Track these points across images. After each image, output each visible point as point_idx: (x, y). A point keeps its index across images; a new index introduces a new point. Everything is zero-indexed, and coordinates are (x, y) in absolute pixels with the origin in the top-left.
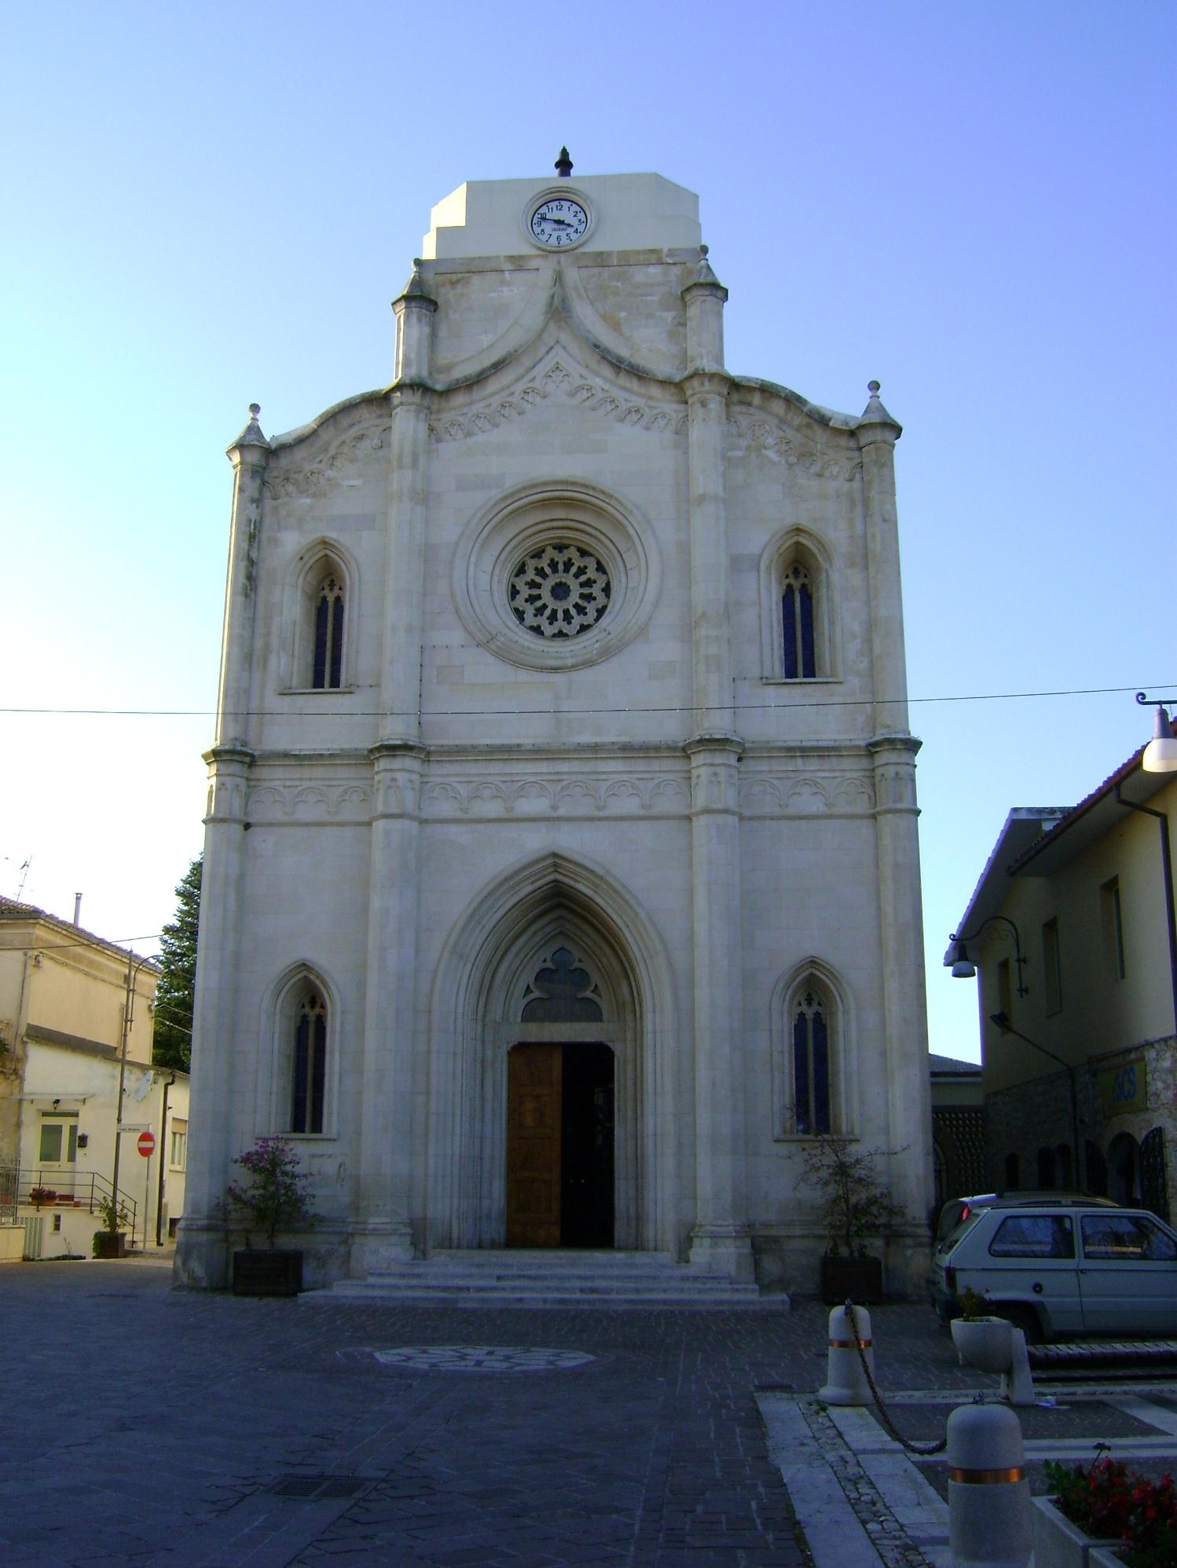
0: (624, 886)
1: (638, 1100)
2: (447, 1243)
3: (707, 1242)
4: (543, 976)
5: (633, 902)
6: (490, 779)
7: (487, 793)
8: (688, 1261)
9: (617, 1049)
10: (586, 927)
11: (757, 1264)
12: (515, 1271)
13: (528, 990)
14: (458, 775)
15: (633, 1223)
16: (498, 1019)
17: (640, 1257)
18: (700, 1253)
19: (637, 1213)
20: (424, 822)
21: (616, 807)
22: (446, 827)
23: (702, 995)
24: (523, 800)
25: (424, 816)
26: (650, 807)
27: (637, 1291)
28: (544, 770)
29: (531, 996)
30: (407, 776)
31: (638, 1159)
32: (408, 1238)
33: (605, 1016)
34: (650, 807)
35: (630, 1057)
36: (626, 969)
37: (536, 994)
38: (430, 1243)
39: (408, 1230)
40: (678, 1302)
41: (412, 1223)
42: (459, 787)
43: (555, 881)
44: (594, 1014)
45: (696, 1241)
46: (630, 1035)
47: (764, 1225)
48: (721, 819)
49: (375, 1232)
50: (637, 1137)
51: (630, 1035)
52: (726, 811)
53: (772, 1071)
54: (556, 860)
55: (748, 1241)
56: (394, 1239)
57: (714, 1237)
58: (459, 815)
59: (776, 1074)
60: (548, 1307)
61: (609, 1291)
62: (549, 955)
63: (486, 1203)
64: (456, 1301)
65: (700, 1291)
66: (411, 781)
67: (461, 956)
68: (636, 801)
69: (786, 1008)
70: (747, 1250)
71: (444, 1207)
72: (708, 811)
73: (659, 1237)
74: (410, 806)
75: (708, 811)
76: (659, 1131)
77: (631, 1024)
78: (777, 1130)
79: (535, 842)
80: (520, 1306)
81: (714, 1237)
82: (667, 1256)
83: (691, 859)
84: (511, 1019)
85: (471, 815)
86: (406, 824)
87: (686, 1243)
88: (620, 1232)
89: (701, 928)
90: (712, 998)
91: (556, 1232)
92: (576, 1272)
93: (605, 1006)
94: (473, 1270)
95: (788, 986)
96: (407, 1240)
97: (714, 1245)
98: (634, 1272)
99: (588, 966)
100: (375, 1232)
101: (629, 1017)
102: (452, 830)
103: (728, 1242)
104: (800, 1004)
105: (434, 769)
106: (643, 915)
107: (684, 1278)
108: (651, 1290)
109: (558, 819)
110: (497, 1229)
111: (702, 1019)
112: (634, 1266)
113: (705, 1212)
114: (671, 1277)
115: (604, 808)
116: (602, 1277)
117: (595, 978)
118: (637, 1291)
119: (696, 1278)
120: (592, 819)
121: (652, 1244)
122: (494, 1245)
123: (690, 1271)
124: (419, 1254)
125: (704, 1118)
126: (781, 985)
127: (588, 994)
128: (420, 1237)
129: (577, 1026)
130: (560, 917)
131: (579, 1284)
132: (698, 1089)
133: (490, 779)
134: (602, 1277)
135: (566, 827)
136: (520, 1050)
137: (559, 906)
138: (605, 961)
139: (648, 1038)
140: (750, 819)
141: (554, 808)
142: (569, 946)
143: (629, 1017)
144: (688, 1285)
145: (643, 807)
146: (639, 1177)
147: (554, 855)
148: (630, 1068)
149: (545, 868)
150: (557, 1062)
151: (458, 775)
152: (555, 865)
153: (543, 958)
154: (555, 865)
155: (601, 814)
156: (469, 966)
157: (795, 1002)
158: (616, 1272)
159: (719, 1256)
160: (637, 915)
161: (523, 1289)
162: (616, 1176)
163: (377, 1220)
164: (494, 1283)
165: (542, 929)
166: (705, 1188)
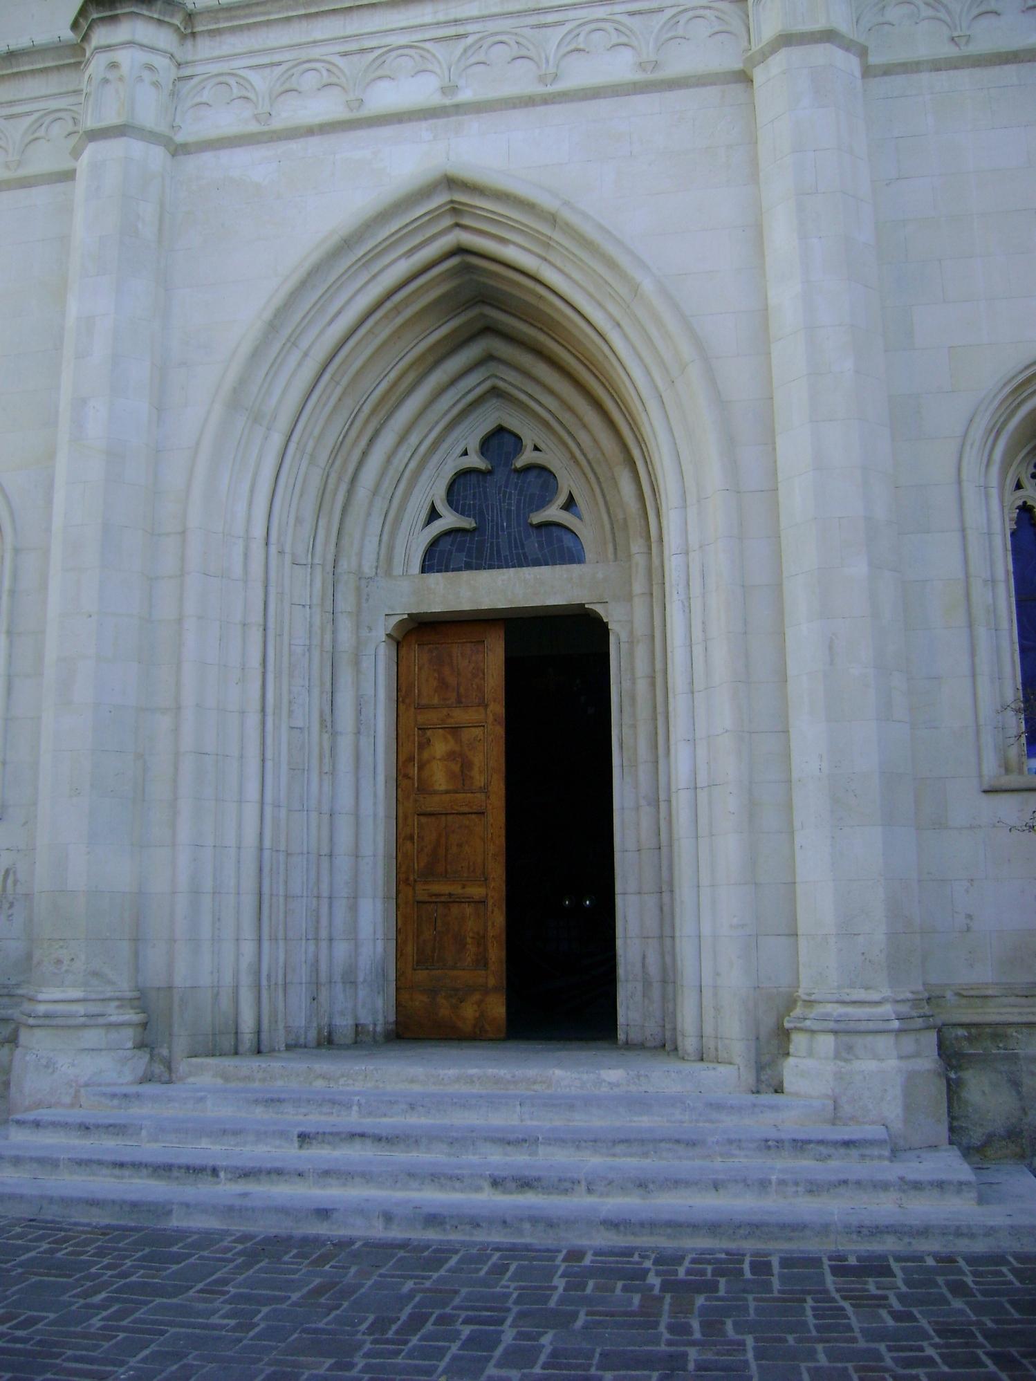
0: (602, 228)
1: (659, 715)
2: (224, 1043)
3: (826, 1043)
4: (461, 487)
5: (623, 260)
6: (316, 52)
7: (310, 81)
8: (779, 1090)
9: (613, 616)
10: (542, 370)
11: (953, 1090)
12: (353, 1119)
13: (433, 515)
14: (252, 53)
15: (656, 993)
16: (368, 570)
17: (662, 1077)
18: (809, 1070)
19: (664, 969)
20: (179, 150)
21: (580, 74)
22: (225, 156)
23: (794, 449)
24: (383, 85)
25: (180, 138)
26: (656, 65)
27: (642, 1185)
28: (428, 19)
29: (439, 526)
30: (143, 57)
31: (662, 848)
32: (129, 1033)
33: (589, 555)
34: (656, 65)
35: (640, 628)
36: (630, 453)
37: (449, 519)
38: (181, 1043)
39: (132, 1016)
40: (755, 1228)
41: (141, 1000)
42: (253, 77)
43: (460, 250)
44: (557, 546)
45: (799, 1041)
46: (638, 587)
47: (970, 996)
48: (822, 54)
49: (50, 1021)
50: (659, 800)
51: (638, 587)
52: (829, 36)
53: (970, 625)
54: (455, 193)
55: (932, 1037)
56: (92, 1037)
57: (845, 1031)
58: (254, 127)
59: (982, 632)
60: (396, 1233)
61: (565, 1184)
62: (473, 443)
63: (342, 949)
64: (162, 1210)
65: (814, 1188)
66: (150, 68)
67: (256, 419)
68: (627, 56)
69: (994, 479)
70: (928, 1062)
71: (214, 961)
72: (787, 40)
73: (708, 1029)
74: (149, 113)
75: (787, 40)
76: (702, 780)
77: (639, 560)
78: (990, 766)
79: (407, 161)
80: (320, 1229)
81: (845, 1031)
82: (727, 1077)
83: (754, 162)
84: (398, 570)
85: (277, 124)
86: (136, 148)
87: (772, 1043)
88: (631, 1008)
89: (785, 299)
90: (818, 457)
91: (497, 1008)
92: (499, 1120)
93: (586, 529)
94: (259, 1112)
95: (996, 431)
96: (128, 1037)
97: (844, 1053)
98: (644, 1121)
99: (552, 458)
100: (50, 1021)
101: (637, 547)
102: (239, 161)
103: (883, 1043)
104: (1019, 486)
105: (205, 48)
106: (648, 286)
107: (770, 1145)
108: (676, 1183)
109: (459, 109)
110: (376, 1007)
111: (797, 499)
112: (640, 1103)
113: (820, 969)
114: (734, 1142)
115: (556, 77)
116: (557, 1139)
117: (568, 481)
118: (642, 1185)
119: (800, 1145)
120: (528, 102)
121: (689, 1044)
122: (362, 1040)
123: (788, 1118)
124: (158, 1068)
125: (809, 736)
126: (982, 423)
127: (553, 512)
128: (155, 1030)
129: (529, 573)
130: (489, 358)
131: (497, 1158)
132: (792, 671)
133: (316, 52)
134: (557, 1139)
135: (473, 124)
136: (420, 632)
137: (490, 330)
138: (582, 436)
139: (674, 565)
140: (888, 71)
141: (448, 89)
142: (515, 422)
143: (637, 547)
144: (781, 1165)
145: (542, 79)
146: (665, 888)
147: (451, 182)
148: (641, 651)
149: (434, 216)
150: (493, 658)
151: (252, 53)
152: (455, 209)
153: (463, 449)
154: (455, 209)
155: (551, 89)
156: (277, 439)
157: (1010, 483)
158: (597, 1121)
159: (862, 1078)
160: (635, 289)
161: (344, 1175)
162: (619, 888)
163: (57, 994)
164: (290, 1153)
165: (453, 382)
166: (818, 906)
